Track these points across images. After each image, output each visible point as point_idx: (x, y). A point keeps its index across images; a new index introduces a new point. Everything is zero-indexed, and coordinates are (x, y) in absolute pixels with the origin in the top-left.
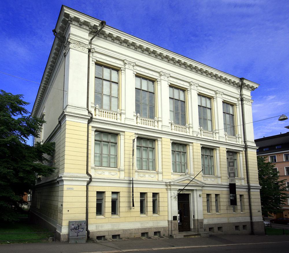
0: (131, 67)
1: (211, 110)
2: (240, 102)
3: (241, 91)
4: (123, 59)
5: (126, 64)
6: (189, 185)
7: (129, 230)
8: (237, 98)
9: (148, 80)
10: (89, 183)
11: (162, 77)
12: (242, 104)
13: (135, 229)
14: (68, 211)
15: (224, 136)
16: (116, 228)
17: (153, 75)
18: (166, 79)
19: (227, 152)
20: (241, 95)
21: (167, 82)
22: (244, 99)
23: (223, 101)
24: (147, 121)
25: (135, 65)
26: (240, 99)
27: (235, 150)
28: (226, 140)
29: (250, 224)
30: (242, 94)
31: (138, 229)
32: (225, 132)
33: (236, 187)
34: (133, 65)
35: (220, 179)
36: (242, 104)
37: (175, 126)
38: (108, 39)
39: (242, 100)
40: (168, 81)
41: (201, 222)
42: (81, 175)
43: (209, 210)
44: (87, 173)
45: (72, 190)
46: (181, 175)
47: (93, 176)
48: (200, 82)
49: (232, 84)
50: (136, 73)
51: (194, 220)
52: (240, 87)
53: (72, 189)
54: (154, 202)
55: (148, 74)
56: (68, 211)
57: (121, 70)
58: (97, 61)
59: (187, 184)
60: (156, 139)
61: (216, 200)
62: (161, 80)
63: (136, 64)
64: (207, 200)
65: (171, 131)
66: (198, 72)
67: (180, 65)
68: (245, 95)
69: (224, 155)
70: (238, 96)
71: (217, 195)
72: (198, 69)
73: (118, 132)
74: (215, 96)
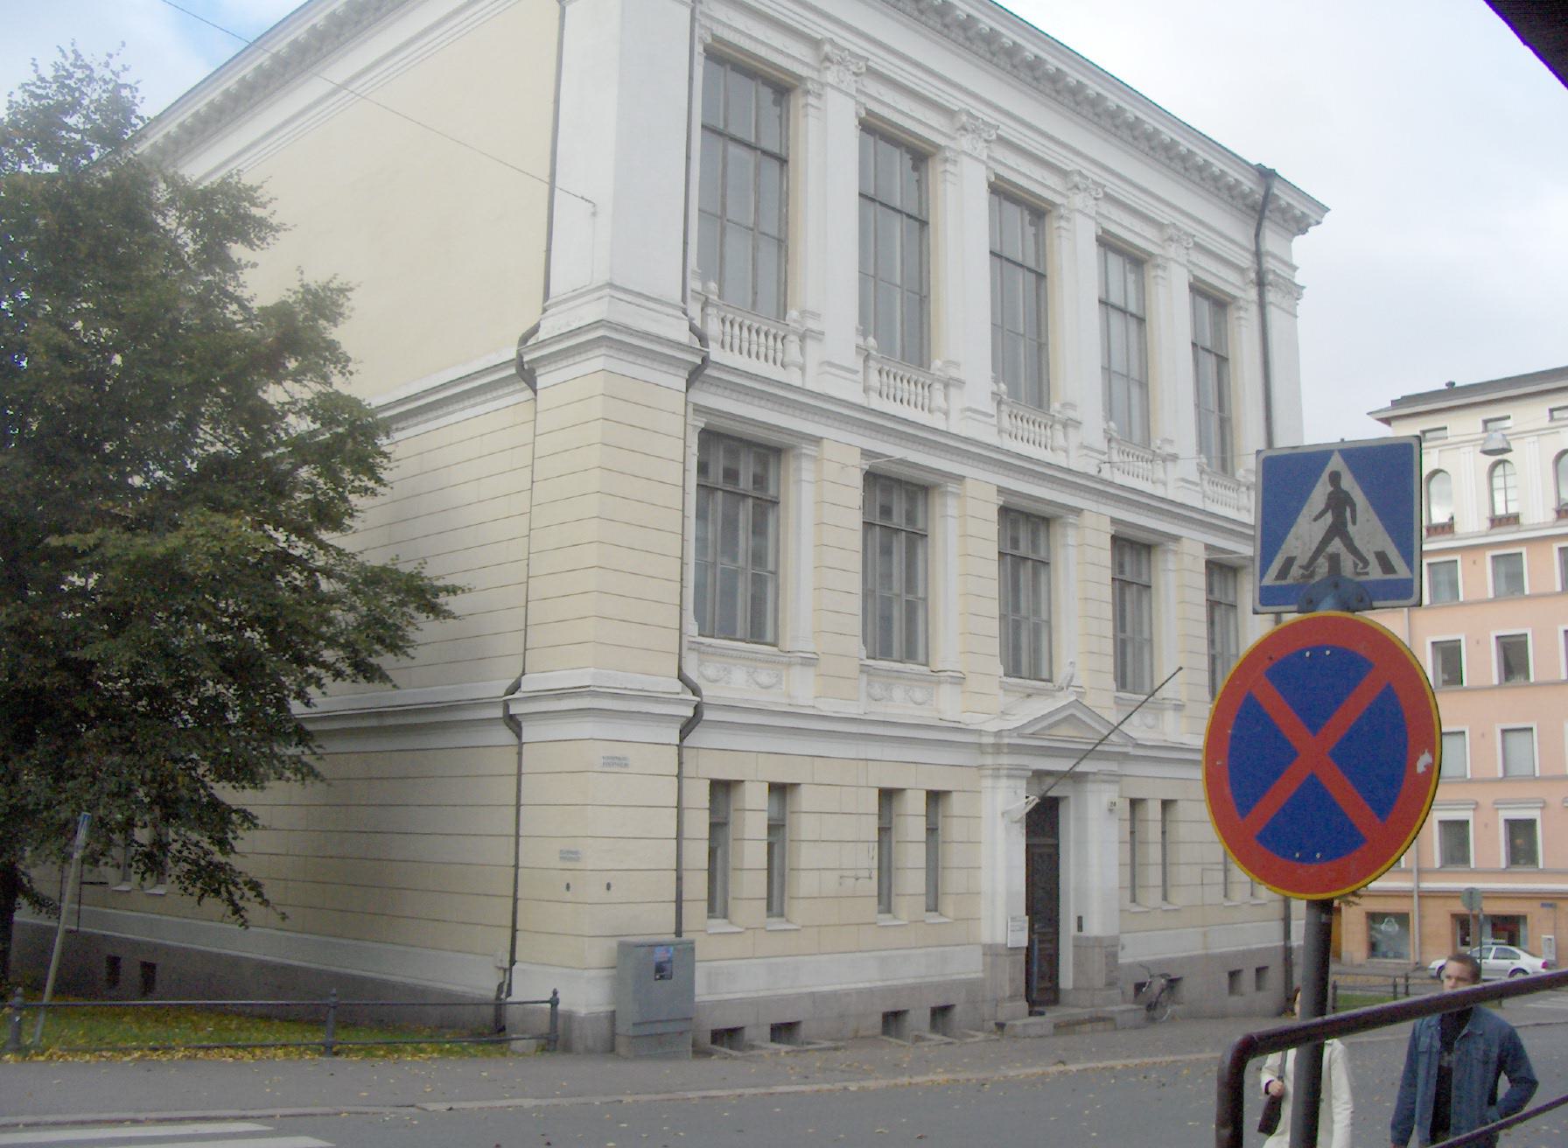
0: (849, 78)
1: (782, 166)
2: (1253, 294)
3: (1257, 235)
4: (819, 37)
5: (828, 64)
6: (1106, 748)
7: (835, 995)
8: (1241, 270)
9: (877, 136)
10: (687, 728)
11: (831, 76)
12: (1262, 306)
13: (860, 992)
14: (609, 887)
15: (992, 408)
16: (786, 988)
17: (788, 55)
18: (982, 150)
19: (1004, 511)
20: (1258, 254)
21: (852, 103)
22: (1271, 277)
23: (993, 179)
24: (758, 333)
25: (864, 70)
26: (1253, 276)
27: (902, 462)
28: (866, 390)
29: (1279, 960)
30: (1263, 249)
31: (871, 991)
32: (865, 335)
33: (1200, 757)
34: (856, 70)
35: (810, 672)
36: (1262, 306)
37: (723, 321)
38: (1022, 75)
39: (1261, 284)
40: (992, 164)
41: (1110, 949)
42: (636, 681)
43: (1134, 887)
44: (681, 677)
45: (623, 770)
46: (1029, 691)
47: (708, 692)
48: (1111, 178)
49: (1179, 167)
50: (866, 109)
51: (1079, 945)
52: (1253, 214)
53: (621, 762)
54: (776, 828)
55: (759, 46)
56: (609, 887)
57: (807, 92)
58: (716, 38)
59: (1090, 747)
60: (792, 447)
61: (932, 830)
62: (823, 85)
63: (870, 63)
64: (880, 829)
65: (859, 399)
66: (953, 36)
67: (1096, 114)
68: (1274, 257)
69: (988, 531)
70: (1246, 260)
71: (935, 798)
72: (1087, 98)
73: (1059, 512)
74: (814, 75)
